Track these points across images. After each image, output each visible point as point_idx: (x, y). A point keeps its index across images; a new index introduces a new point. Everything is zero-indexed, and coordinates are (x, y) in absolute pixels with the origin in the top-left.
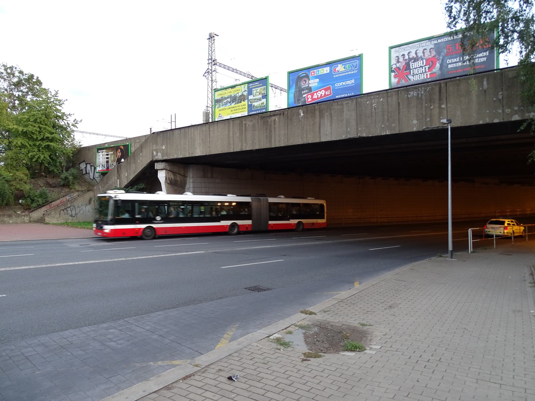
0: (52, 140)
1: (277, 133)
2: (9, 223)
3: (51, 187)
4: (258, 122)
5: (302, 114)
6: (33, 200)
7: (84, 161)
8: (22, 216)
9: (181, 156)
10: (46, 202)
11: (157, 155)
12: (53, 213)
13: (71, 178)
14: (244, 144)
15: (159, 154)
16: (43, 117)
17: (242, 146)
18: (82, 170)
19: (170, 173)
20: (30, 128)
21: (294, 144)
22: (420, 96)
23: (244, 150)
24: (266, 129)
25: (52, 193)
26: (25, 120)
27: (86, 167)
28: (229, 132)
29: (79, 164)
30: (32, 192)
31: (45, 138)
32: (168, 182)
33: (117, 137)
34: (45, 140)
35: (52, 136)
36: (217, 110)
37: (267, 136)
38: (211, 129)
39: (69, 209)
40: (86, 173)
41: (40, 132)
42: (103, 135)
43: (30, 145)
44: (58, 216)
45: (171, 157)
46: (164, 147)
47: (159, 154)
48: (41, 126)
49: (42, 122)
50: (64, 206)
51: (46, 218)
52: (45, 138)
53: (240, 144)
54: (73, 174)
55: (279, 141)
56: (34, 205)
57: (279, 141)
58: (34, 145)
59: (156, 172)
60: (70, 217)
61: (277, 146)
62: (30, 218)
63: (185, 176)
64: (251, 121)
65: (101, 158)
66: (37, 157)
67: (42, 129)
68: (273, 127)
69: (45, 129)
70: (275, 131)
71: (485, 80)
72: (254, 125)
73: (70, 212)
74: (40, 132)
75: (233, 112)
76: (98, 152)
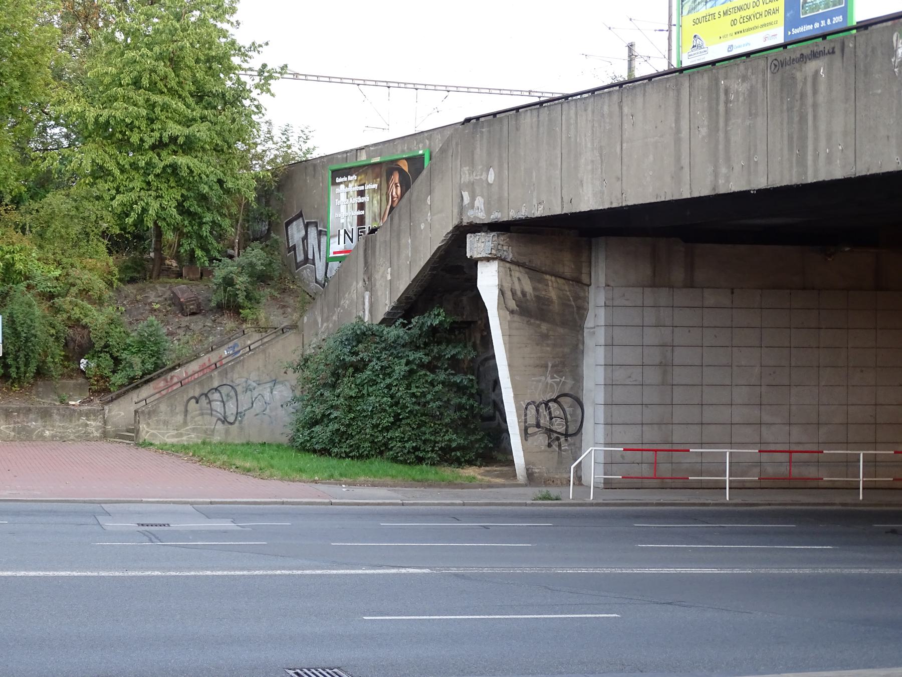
0: (188, 146)
1: (822, 127)
2: (41, 437)
3: (184, 314)
4: (764, 82)
6: (117, 361)
7: (300, 215)
8: (81, 414)
10: (157, 367)
12: (163, 407)
13: (242, 281)
14: (723, 170)
15: (479, 202)
16: (162, 68)
17: (716, 174)
18: (294, 248)
19: (517, 272)
20: (119, 111)
21: (875, 170)
23: (722, 191)
24: (790, 109)
25: (178, 336)
26: (107, 80)
27: (305, 238)
28: (677, 120)
29: (288, 224)
30: (116, 332)
31: (166, 139)
32: (512, 304)
33: (511, 93)
34: (166, 145)
35: (187, 131)
36: (688, 20)
37: (790, 138)
38: (626, 110)
39: (216, 396)
40: (306, 260)
41: (151, 121)
42: (435, 88)
43: (123, 171)
44: (180, 418)
45: (523, 213)
46: (491, 178)
47: (479, 202)
48: (155, 98)
49: (160, 85)
50: (201, 384)
51: (143, 426)
52: (166, 139)
53: (710, 169)
54: (252, 265)
55: (829, 159)
56: (118, 379)
57: (829, 159)
58: (134, 166)
60: (220, 426)
61: (823, 176)
62: (105, 423)
63: (579, 282)
64: (744, 78)
65: (343, 205)
66: (138, 208)
67: (158, 110)
68: (810, 101)
69: (165, 107)
70: (815, 117)
72: (752, 92)
73: (217, 406)
74: (151, 121)
75: (739, 27)
76: (334, 183)
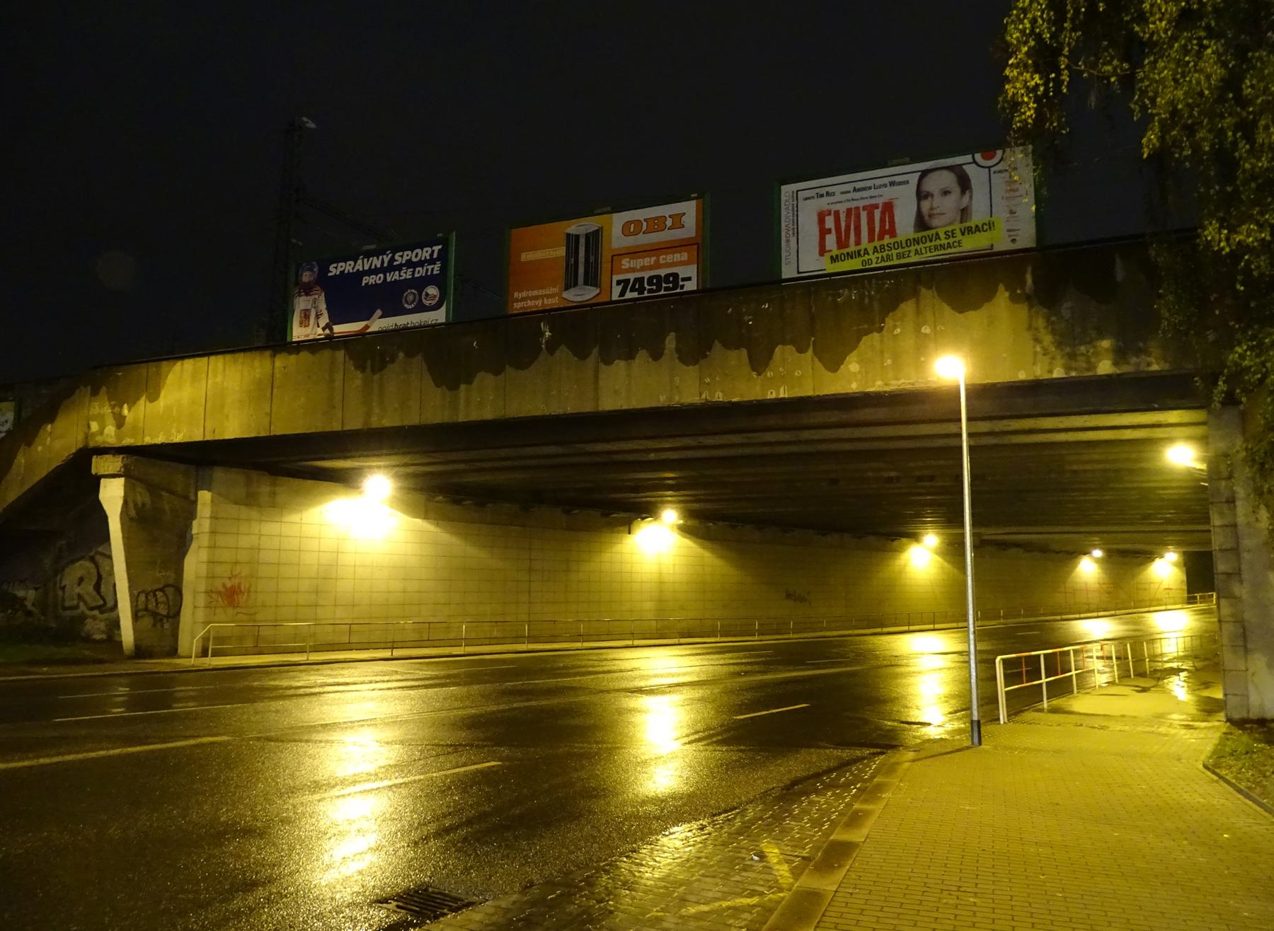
5: (548, 334)
9: (178, 438)
11: (101, 432)
22: (867, 301)
32: (133, 513)
45: (148, 440)
59: (95, 483)
71: (127, 634)
